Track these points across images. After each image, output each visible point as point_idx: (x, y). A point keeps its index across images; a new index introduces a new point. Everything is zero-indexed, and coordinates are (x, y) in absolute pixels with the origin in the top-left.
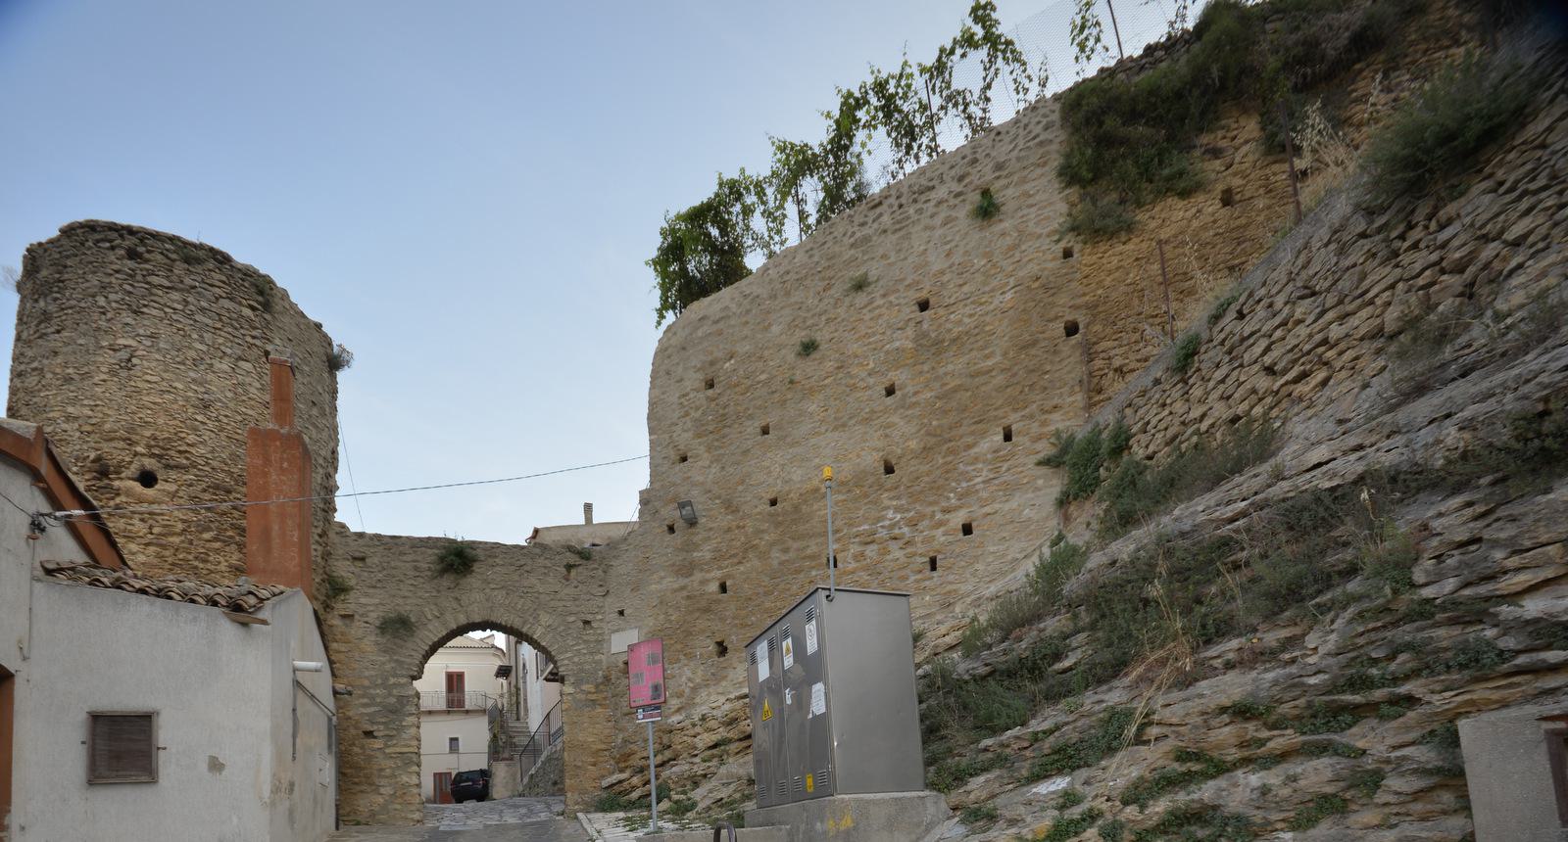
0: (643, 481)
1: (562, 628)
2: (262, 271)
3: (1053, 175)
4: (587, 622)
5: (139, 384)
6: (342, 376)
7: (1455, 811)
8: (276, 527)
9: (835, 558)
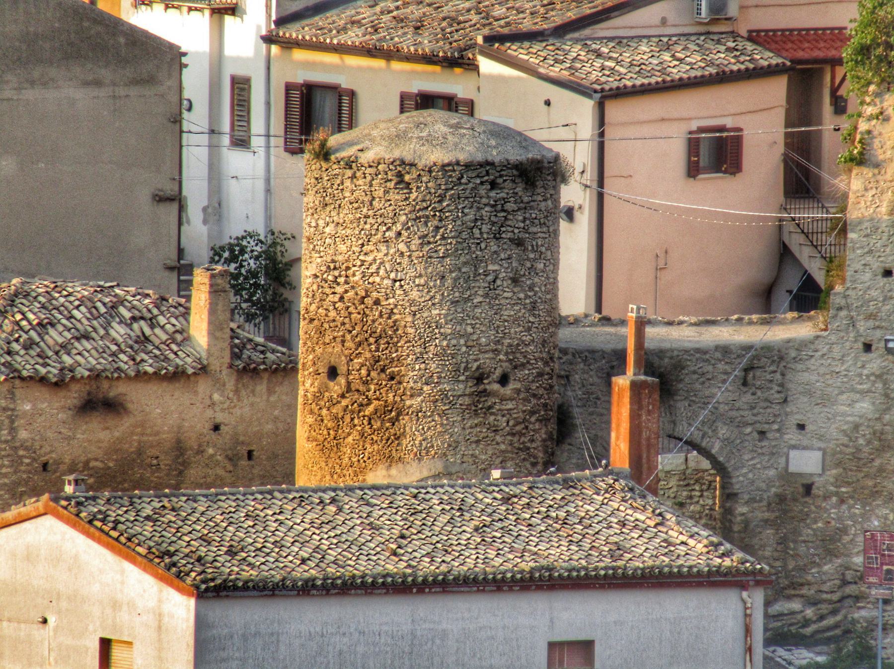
0: (343, 86)
1: (738, 441)
2: (561, 250)
3: (159, 186)
4: (762, 433)
5: (502, 301)
6: (184, 71)
7: (103, 613)
8: (645, 456)
9: (450, 103)
